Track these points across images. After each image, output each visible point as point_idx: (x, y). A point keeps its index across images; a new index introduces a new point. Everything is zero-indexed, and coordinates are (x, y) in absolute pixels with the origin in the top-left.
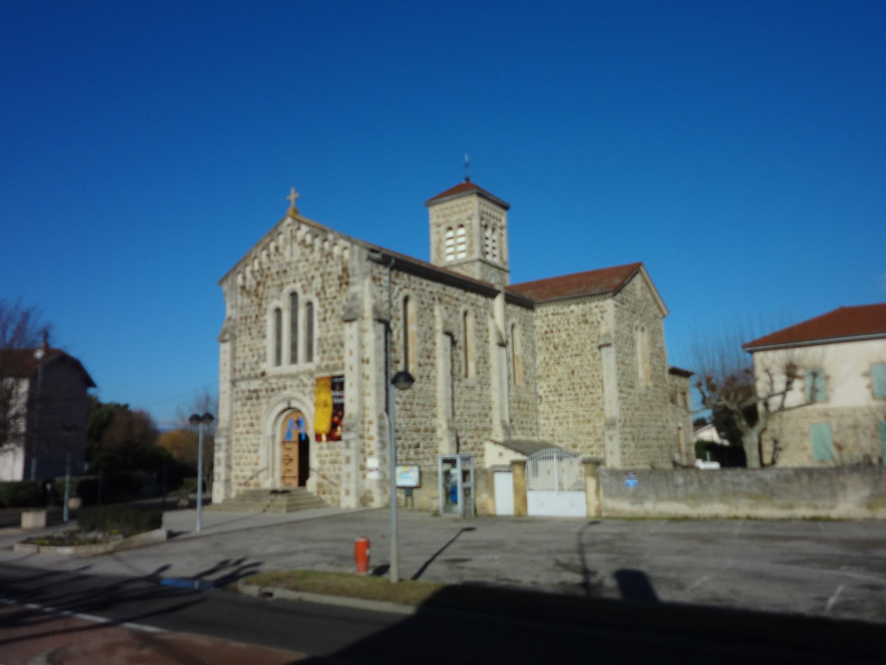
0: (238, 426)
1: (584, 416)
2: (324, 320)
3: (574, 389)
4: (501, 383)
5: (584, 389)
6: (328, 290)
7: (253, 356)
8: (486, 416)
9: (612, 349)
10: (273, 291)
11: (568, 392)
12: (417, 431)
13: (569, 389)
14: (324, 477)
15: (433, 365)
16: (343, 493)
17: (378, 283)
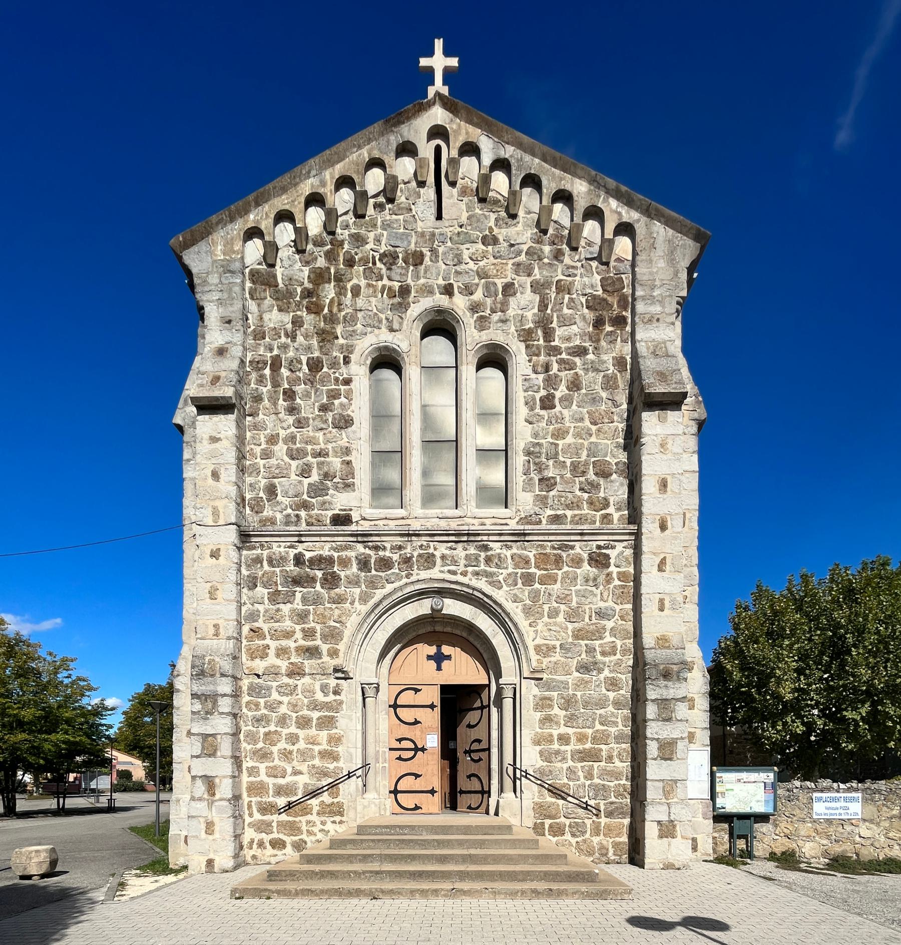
2: (547, 403)
14: (557, 792)
17: (577, 382)
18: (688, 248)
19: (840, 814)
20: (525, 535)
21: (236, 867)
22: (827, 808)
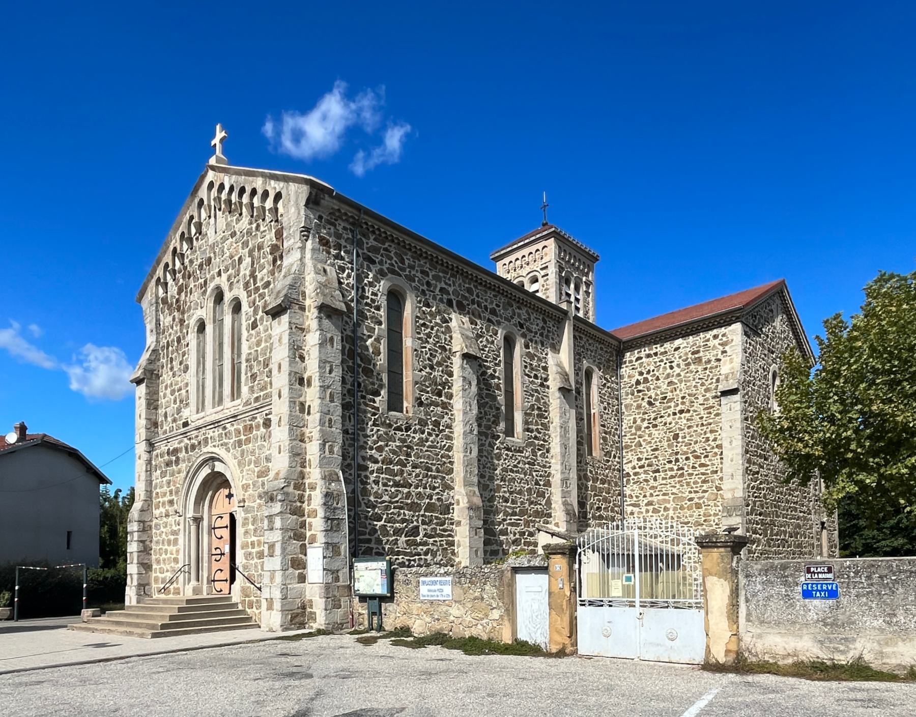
0: (158, 507)
1: (691, 499)
3: (677, 460)
4: (565, 446)
5: (692, 460)
6: (259, 275)
7: (175, 401)
8: (542, 495)
9: (737, 397)
10: (195, 296)
11: (668, 466)
12: (414, 507)
13: (670, 462)
15: (445, 406)
16: (264, 604)
18: (374, 149)
19: (438, 596)
20: (237, 416)
21: (561, 654)
22: (429, 591)
